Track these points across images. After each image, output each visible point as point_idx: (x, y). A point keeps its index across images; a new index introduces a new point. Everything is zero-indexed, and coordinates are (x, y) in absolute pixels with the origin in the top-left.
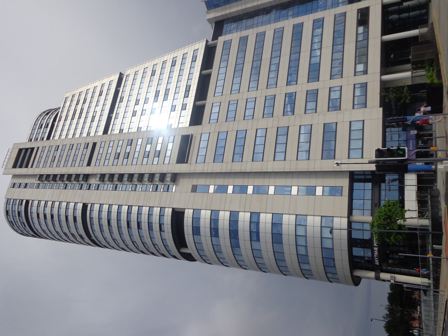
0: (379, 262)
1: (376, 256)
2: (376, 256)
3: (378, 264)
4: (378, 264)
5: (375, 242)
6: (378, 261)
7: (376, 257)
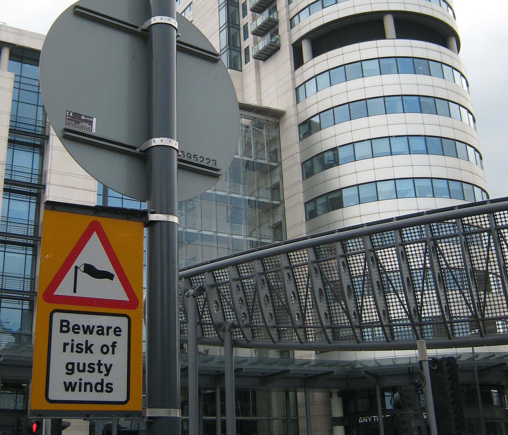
0: (25, 384)
1: (375, 419)
2: (375, 419)
4: (360, 422)
6: (366, 421)
7: (372, 419)
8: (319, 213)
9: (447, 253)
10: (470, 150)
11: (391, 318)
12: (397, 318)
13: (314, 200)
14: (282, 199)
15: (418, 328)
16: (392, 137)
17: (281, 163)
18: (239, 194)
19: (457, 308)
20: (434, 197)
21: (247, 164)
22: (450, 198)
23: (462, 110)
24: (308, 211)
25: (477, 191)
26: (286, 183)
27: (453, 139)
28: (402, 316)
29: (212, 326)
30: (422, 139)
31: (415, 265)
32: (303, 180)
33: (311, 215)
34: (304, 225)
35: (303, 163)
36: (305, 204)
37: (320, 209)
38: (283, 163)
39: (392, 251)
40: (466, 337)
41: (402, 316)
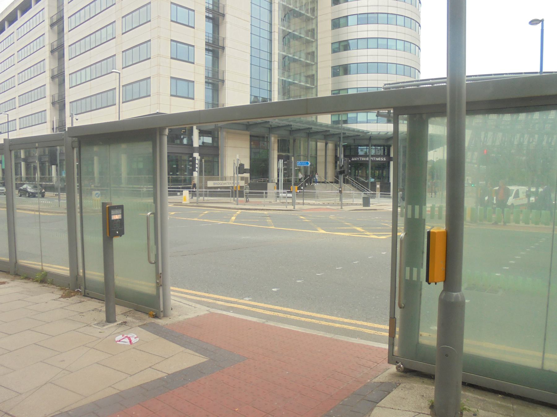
3: (352, 160)
4: (352, 160)
5: (374, 159)
7: (359, 159)
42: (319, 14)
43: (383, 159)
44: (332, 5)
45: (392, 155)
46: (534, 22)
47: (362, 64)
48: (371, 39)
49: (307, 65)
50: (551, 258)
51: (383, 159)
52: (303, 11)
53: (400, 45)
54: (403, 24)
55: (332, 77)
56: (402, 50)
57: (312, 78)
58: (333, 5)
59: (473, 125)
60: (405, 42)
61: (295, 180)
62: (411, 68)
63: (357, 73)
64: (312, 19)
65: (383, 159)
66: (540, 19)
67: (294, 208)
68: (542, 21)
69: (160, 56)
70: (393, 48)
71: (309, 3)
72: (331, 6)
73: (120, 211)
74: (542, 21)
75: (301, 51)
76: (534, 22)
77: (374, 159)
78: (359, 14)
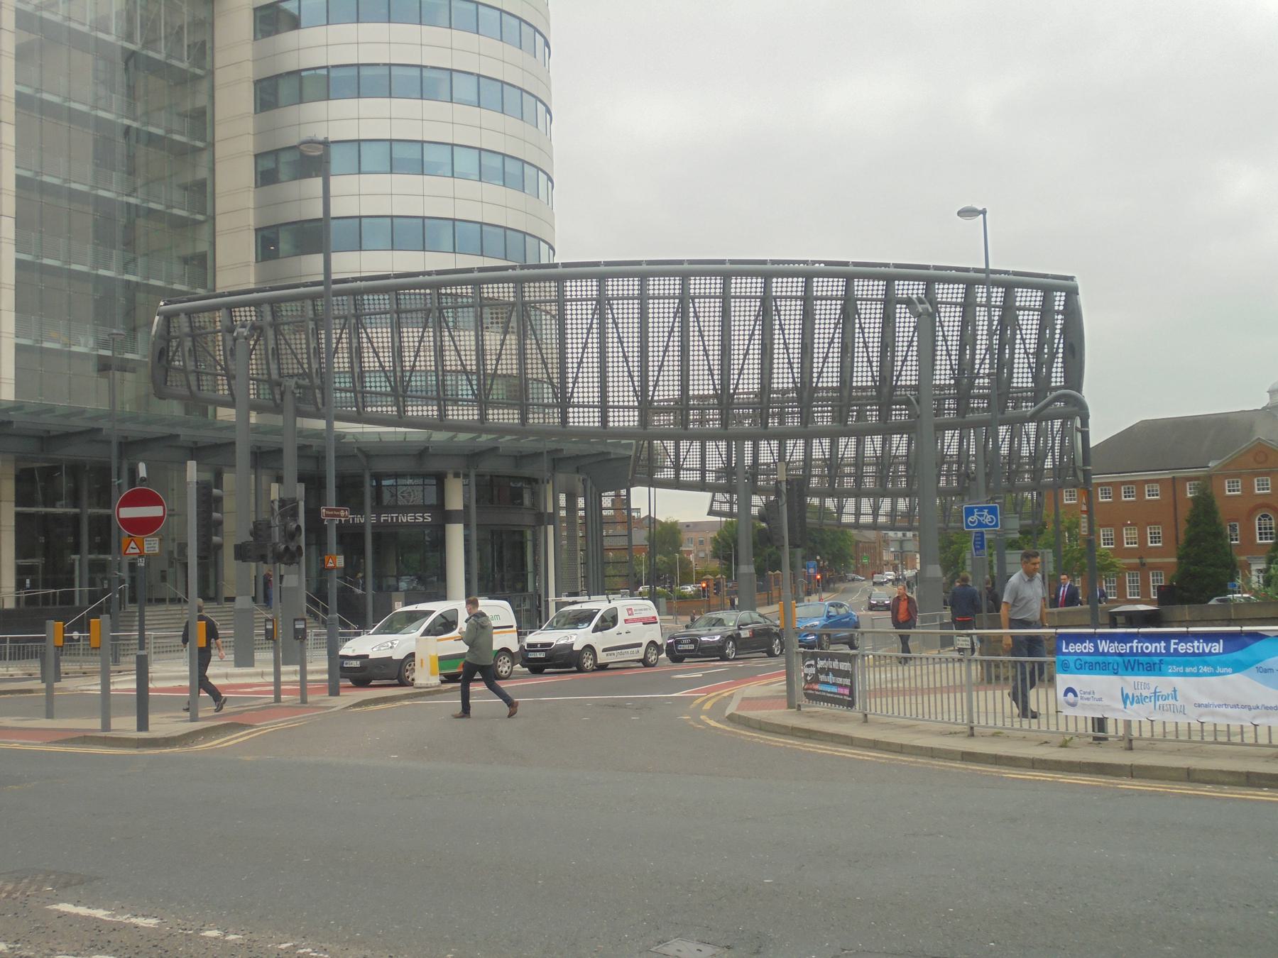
5: (392, 518)
8: (282, 176)
9: (537, 364)
10: (542, 177)
11: (365, 367)
12: (372, 369)
13: (276, 153)
14: (209, 139)
15: (359, 395)
16: (426, 67)
17: (212, 73)
18: (110, 112)
19: (616, 394)
20: (480, 180)
21: (130, 56)
22: (504, 185)
23: (539, 104)
24: (260, 169)
25: (544, 247)
26: (222, 111)
27: (519, 88)
28: (374, 367)
29: (225, 378)
30: (474, 79)
31: (594, 412)
32: (256, 112)
33: (266, 178)
34: (252, 194)
35: (257, 81)
36: (257, 156)
37: (284, 171)
38: (218, 73)
39: (594, 412)
40: (465, 421)
41: (374, 367)
42: (217, 65)
43: (424, 518)
44: (255, 36)
45: (1079, 435)
46: (967, 213)
47: (380, 220)
48: (402, 143)
49: (182, 225)
50: (1175, 509)
51: (424, 518)
52: (159, 52)
53: (466, 161)
54: (474, 98)
55: (257, 261)
56: (473, 177)
57: (202, 265)
58: (259, 36)
59: (795, 395)
60: (506, 158)
61: (314, 586)
62: (527, 237)
63: (361, 247)
64: (197, 78)
65: (421, 520)
66: (980, 208)
67: (106, 726)
68: (984, 212)
69: (455, 308)
70: (440, 172)
71: (181, 28)
72: (252, 38)
73: (303, 622)
74: (984, 212)
75: (171, 176)
76: (967, 213)
77: (392, 518)
78: (333, 66)
